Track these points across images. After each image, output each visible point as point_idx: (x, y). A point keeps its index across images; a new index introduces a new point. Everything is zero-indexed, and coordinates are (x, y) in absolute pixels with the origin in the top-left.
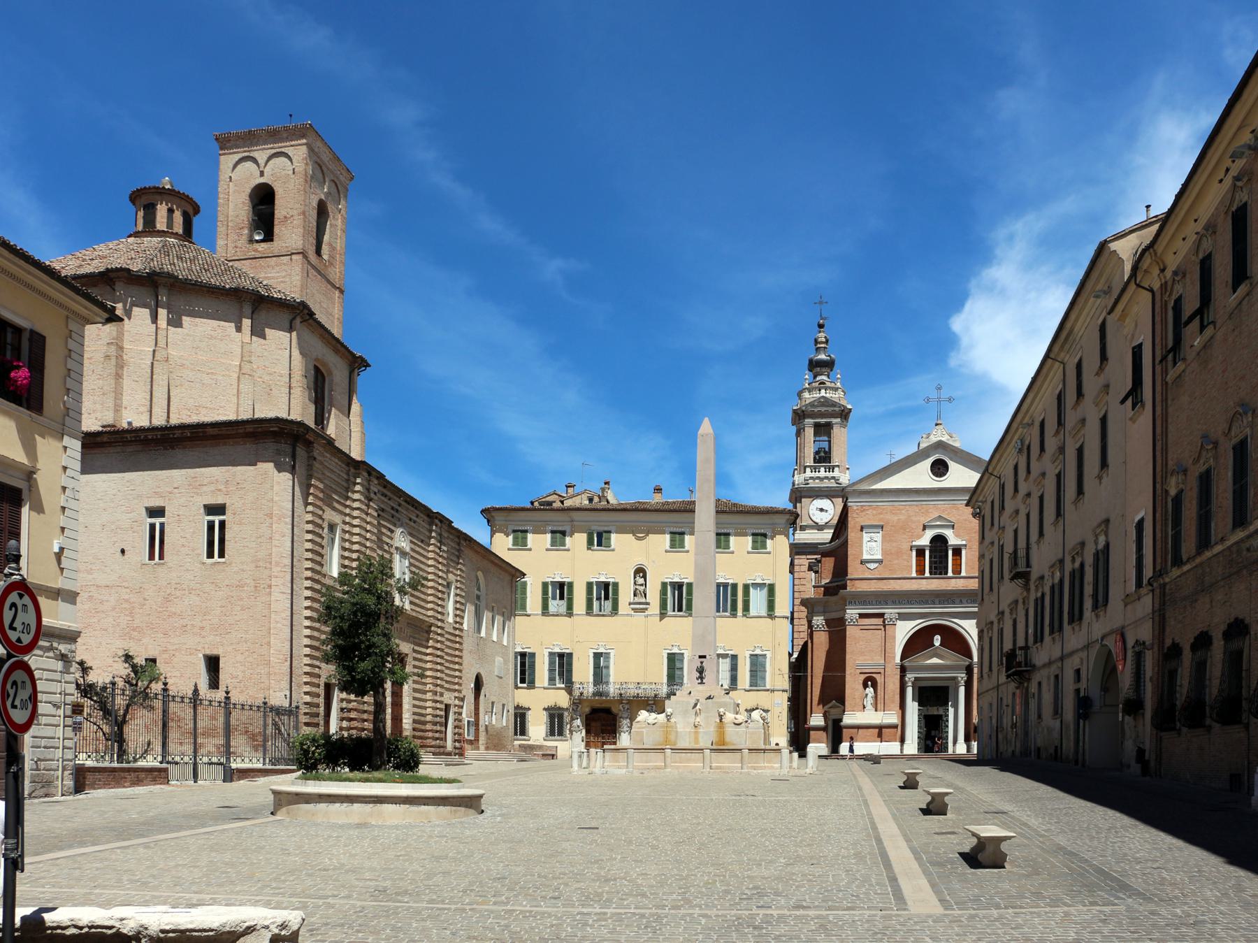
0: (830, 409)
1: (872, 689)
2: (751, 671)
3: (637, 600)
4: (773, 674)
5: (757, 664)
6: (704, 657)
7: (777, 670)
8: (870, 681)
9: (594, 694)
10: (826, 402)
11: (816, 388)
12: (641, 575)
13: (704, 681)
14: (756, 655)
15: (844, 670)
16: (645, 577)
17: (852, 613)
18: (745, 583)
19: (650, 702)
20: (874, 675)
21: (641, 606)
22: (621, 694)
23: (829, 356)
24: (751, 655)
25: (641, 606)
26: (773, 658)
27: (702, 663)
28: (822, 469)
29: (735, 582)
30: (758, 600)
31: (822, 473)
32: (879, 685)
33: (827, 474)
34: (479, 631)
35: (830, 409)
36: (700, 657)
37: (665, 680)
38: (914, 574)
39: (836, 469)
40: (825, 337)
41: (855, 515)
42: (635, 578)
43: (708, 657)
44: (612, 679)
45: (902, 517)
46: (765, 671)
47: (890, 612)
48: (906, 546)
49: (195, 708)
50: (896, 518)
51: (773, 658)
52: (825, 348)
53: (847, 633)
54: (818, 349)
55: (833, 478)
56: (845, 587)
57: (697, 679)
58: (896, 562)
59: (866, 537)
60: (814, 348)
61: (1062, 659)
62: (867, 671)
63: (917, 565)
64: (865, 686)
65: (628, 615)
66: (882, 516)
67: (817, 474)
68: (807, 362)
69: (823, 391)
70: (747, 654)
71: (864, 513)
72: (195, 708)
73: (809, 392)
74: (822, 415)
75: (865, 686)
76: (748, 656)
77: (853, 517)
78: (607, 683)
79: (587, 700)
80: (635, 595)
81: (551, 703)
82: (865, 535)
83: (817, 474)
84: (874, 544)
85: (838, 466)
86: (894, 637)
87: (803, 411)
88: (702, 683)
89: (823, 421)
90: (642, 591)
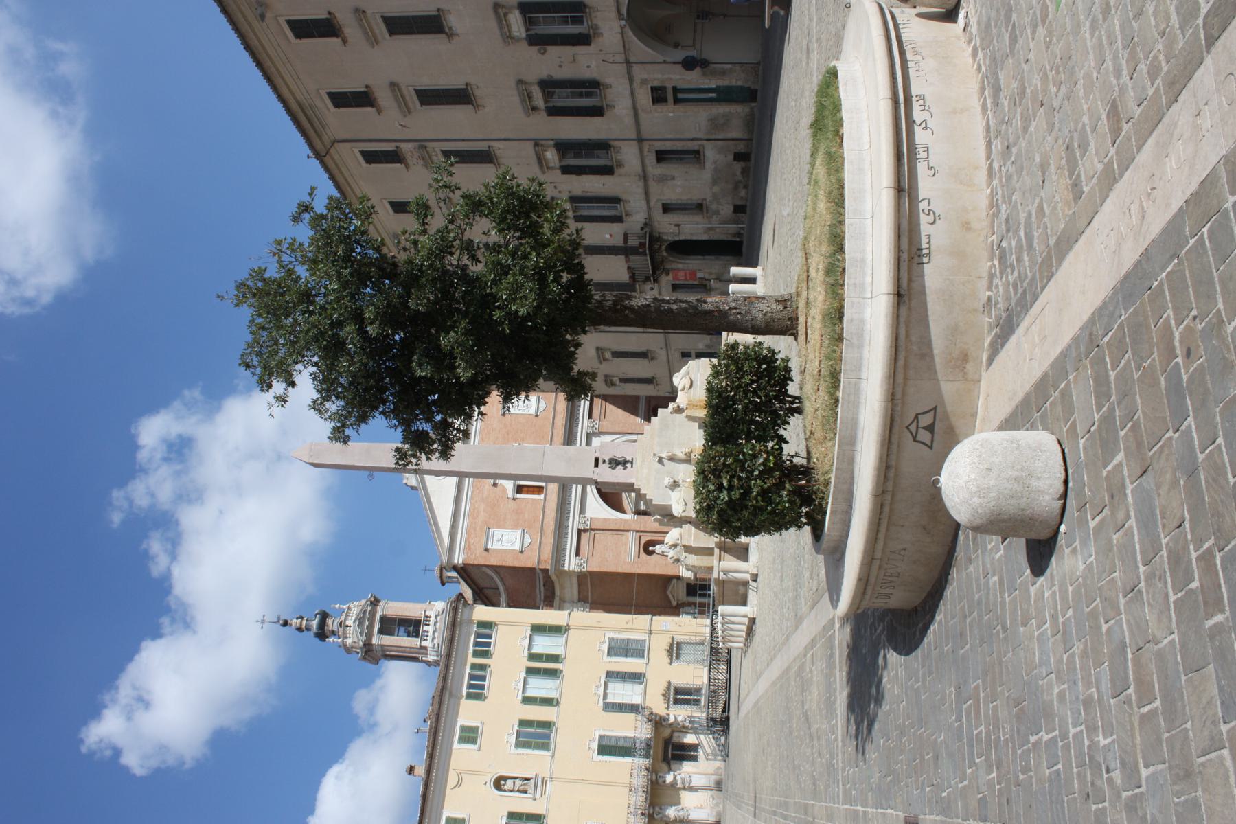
0: (368, 616)
1: (658, 547)
2: (626, 656)
3: (531, 791)
4: (632, 630)
5: (618, 648)
6: (597, 460)
7: (626, 626)
8: (648, 548)
9: (647, 756)
10: (360, 620)
11: (344, 630)
12: (502, 782)
13: (629, 458)
14: (609, 649)
15: (635, 613)
16: (505, 778)
17: (571, 563)
18: (526, 659)
19: (654, 778)
20: (642, 543)
21: (539, 784)
22: (643, 814)
23: (316, 615)
24: (609, 655)
25: (539, 784)
26: (614, 629)
27: (604, 462)
28: (426, 628)
29: (524, 670)
30: (544, 645)
31: (430, 628)
32: (653, 538)
33: (432, 623)
34: (290, 42)
35: (368, 616)
36: (596, 465)
37: (628, 760)
38: (542, 497)
39: (427, 613)
40: (297, 618)
41: (473, 557)
42: (505, 791)
43: (597, 455)
44: (631, 735)
45: (482, 506)
46: (628, 640)
47: (574, 524)
48: (512, 504)
49: (644, 170)
50: (482, 513)
51: (614, 629)
52: (307, 620)
53: (595, 569)
54: (308, 629)
55: (436, 616)
56: (545, 571)
57: (625, 468)
58: (526, 516)
59: (496, 546)
60: (305, 632)
61: (640, 140)
62: (637, 550)
63: (533, 493)
64: (653, 552)
65: (548, 802)
66: (478, 529)
67: (430, 634)
68: (317, 639)
69: (348, 623)
70: (607, 659)
71: (472, 547)
72: (644, 170)
73: (346, 637)
74: (371, 626)
75: (653, 552)
76: (610, 659)
77: (475, 559)
78: (634, 739)
79: (653, 765)
80: (526, 792)
81: (665, 658)
82: (494, 547)
83: (430, 634)
84: (504, 538)
85: (425, 611)
86: (605, 520)
87: (364, 645)
88: (632, 463)
89: (377, 625)
90: (522, 783)
